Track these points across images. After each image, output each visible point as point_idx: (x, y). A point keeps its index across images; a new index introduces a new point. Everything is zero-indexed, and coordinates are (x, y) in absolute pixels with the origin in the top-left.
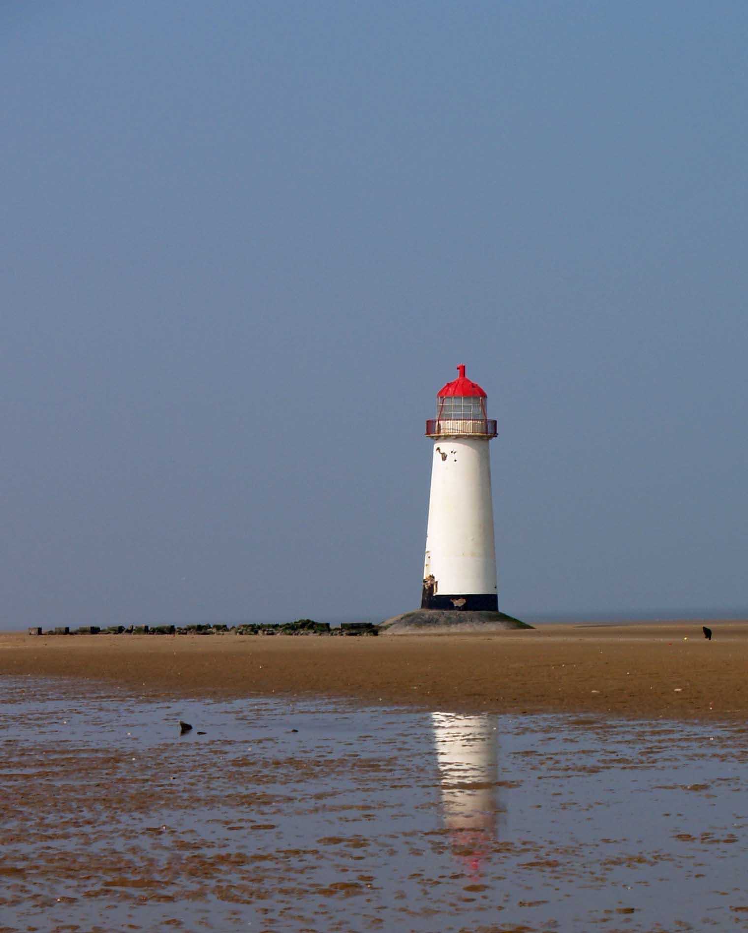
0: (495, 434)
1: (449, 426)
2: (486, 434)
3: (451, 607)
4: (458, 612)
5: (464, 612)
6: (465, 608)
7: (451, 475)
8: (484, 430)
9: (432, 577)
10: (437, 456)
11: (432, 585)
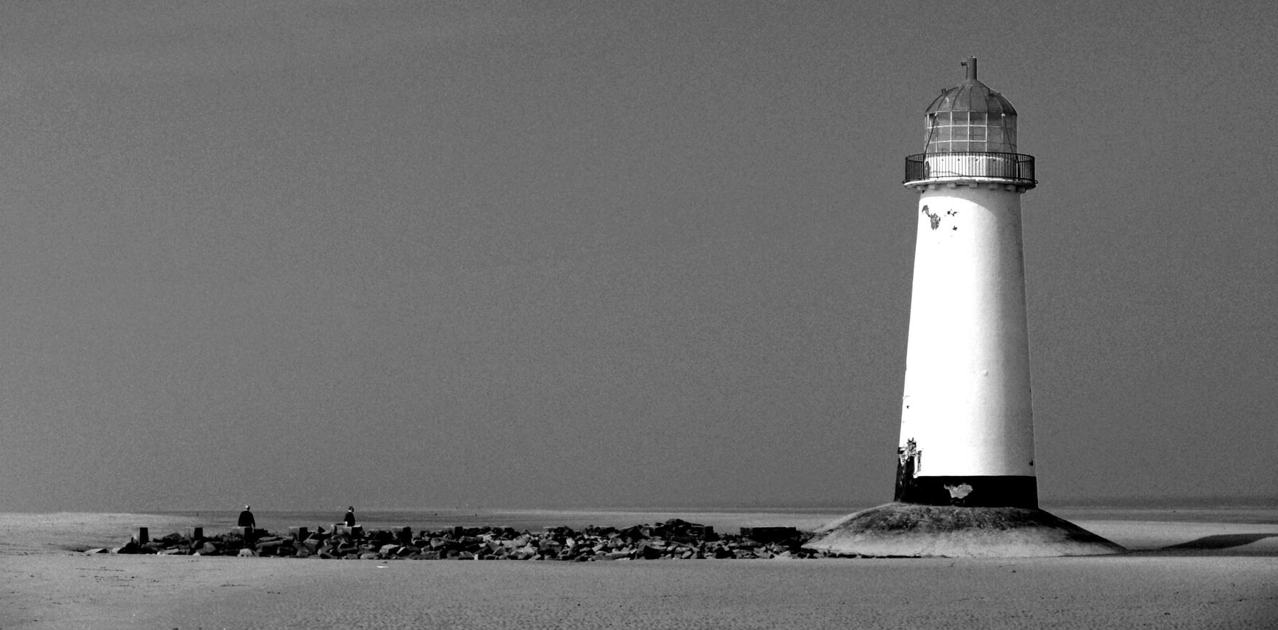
0: (1032, 185)
1: (943, 166)
2: (1013, 182)
3: (945, 500)
4: (958, 509)
5: (968, 510)
6: (968, 502)
7: (953, 257)
8: (1009, 173)
9: (912, 443)
10: (923, 221)
11: (912, 458)
